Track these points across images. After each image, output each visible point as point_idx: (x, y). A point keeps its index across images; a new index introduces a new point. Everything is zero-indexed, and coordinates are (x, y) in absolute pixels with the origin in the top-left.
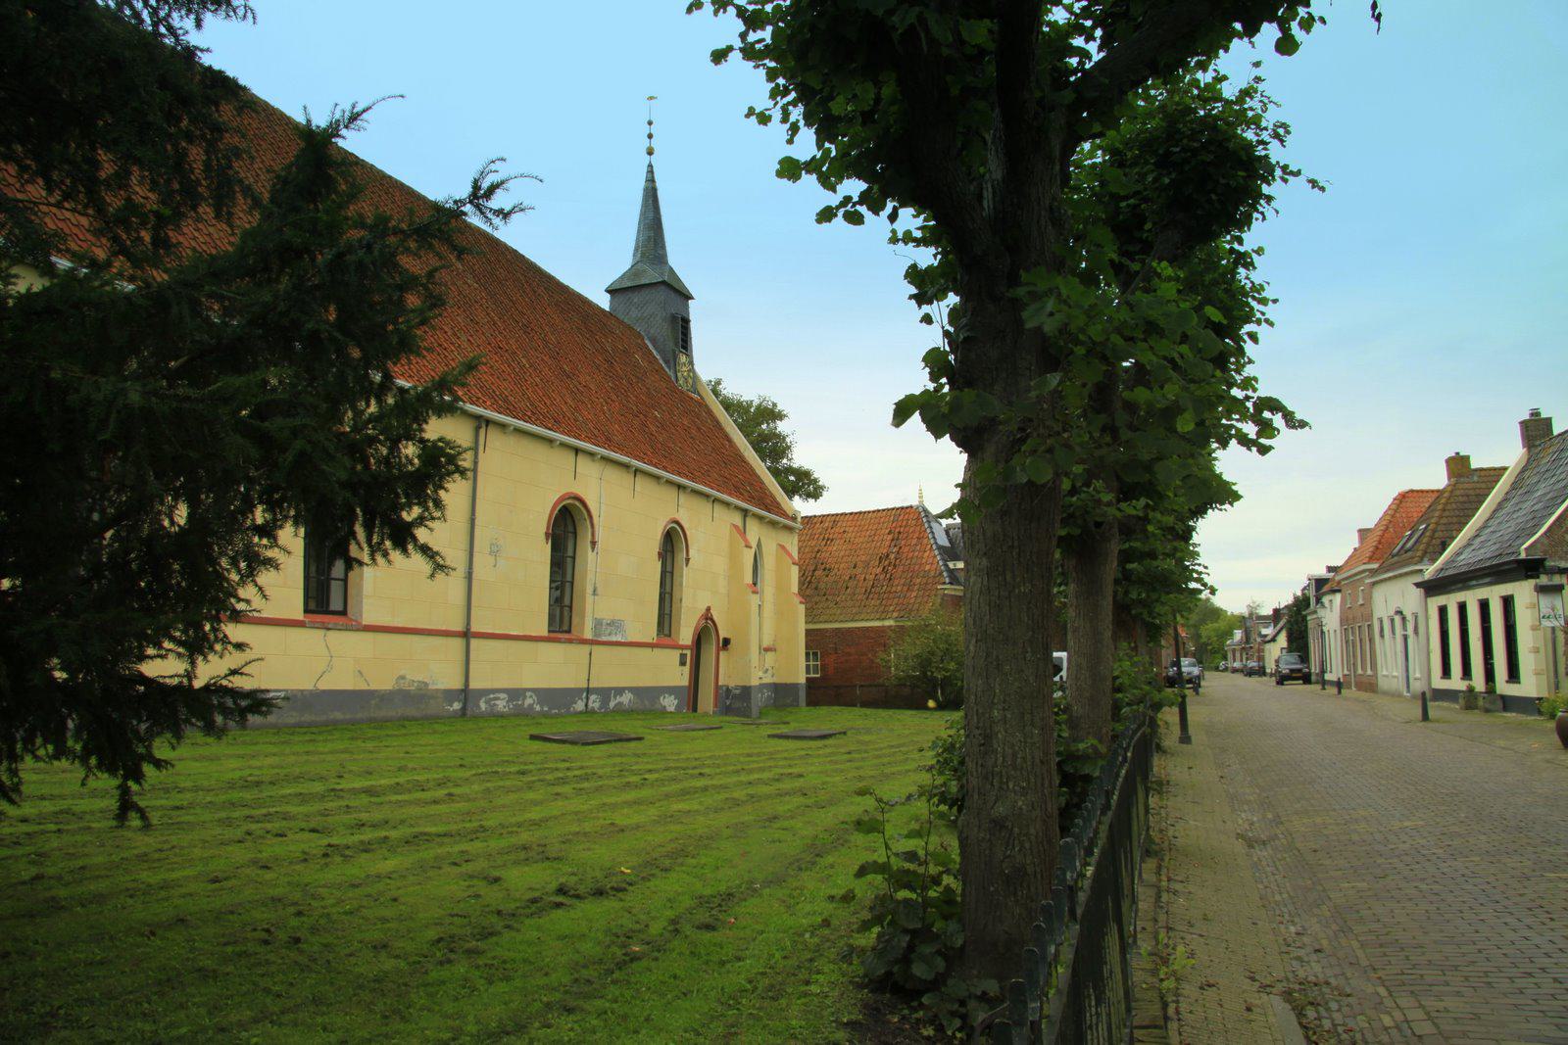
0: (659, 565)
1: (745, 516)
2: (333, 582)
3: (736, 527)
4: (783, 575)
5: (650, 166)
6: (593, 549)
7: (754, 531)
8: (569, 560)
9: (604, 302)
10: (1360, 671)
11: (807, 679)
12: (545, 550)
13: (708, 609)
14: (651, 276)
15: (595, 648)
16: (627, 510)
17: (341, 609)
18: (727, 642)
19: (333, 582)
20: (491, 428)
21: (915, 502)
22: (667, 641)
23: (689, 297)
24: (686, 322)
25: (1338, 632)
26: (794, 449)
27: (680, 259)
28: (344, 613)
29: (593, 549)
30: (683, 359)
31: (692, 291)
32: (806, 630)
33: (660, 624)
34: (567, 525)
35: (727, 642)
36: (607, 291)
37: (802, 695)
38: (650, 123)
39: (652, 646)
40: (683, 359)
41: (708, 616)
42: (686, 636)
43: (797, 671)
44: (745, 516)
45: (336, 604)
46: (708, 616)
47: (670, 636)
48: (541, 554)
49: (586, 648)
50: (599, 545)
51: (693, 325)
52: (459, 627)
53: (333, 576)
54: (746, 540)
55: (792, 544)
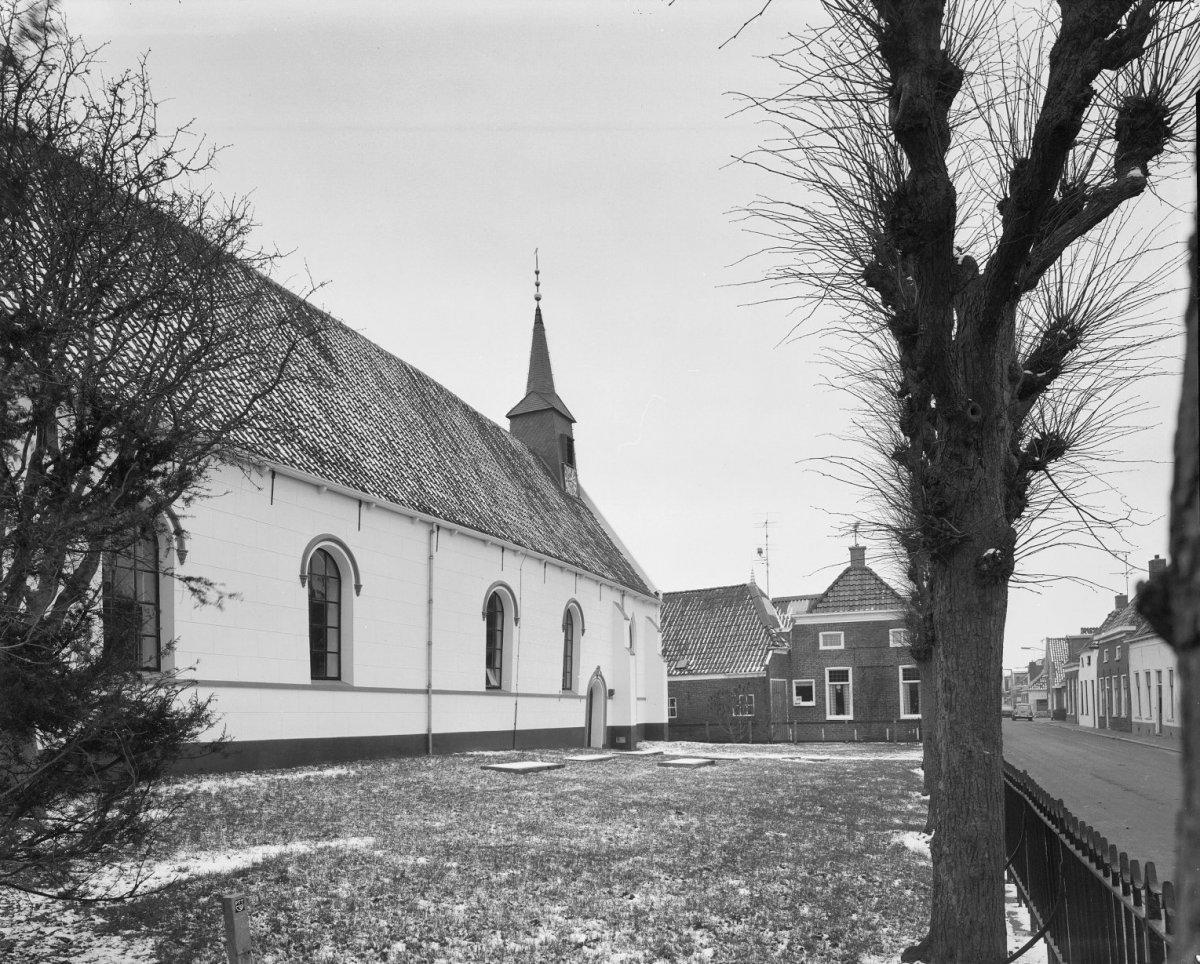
0: (563, 634)
1: (623, 595)
2: (330, 605)
3: (617, 604)
4: (650, 641)
5: (538, 310)
6: (358, 594)
7: (629, 603)
8: (499, 633)
9: (505, 424)
10: (1114, 714)
11: (669, 720)
12: (484, 625)
13: (599, 668)
14: (537, 405)
15: (520, 699)
16: (541, 593)
17: (336, 676)
18: (611, 693)
19: (328, 655)
20: (442, 533)
21: (747, 581)
22: (567, 692)
23: (572, 421)
24: (570, 441)
25: (1095, 683)
26: (410, 525)
27: (567, 388)
28: (338, 678)
29: (358, 594)
30: (568, 470)
31: (575, 416)
32: (669, 682)
33: (564, 681)
34: (496, 610)
35: (611, 693)
36: (508, 416)
37: (666, 731)
38: (537, 273)
39: (560, 697)
40: (568, 470)
41: (598, 673)
42: (582, 688)
43: (662, 716)
44: (623, 595)
45: (332, 671)
46: (598, 673)
47: (570, 689)
48: (434, 598)
49: (514, 699)
50: (521, 621)
51: (575, 443)
52: (423, 687)
53: (329, 624)
54: (624, 614)
55: (656, 614)
